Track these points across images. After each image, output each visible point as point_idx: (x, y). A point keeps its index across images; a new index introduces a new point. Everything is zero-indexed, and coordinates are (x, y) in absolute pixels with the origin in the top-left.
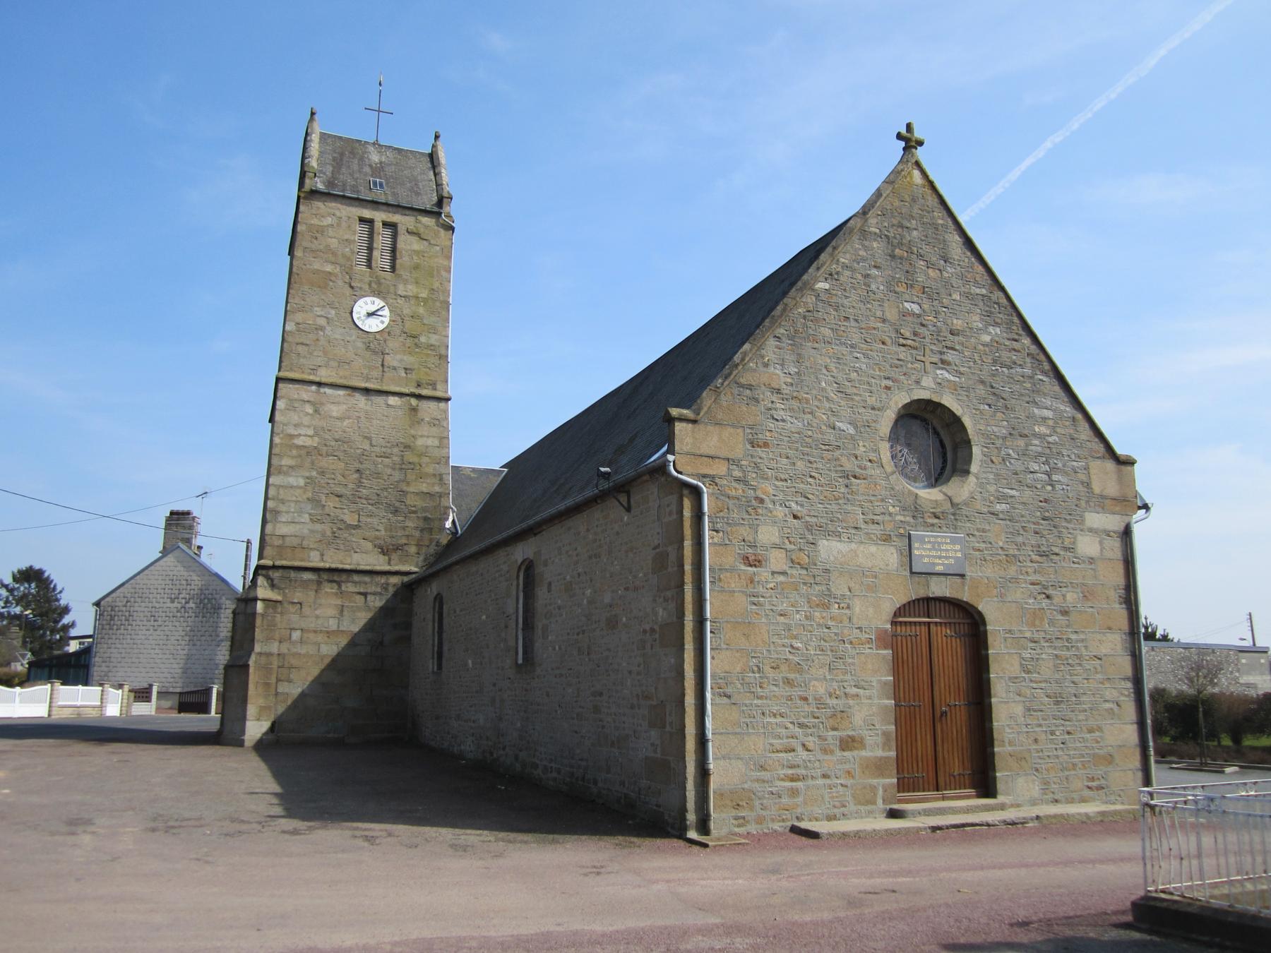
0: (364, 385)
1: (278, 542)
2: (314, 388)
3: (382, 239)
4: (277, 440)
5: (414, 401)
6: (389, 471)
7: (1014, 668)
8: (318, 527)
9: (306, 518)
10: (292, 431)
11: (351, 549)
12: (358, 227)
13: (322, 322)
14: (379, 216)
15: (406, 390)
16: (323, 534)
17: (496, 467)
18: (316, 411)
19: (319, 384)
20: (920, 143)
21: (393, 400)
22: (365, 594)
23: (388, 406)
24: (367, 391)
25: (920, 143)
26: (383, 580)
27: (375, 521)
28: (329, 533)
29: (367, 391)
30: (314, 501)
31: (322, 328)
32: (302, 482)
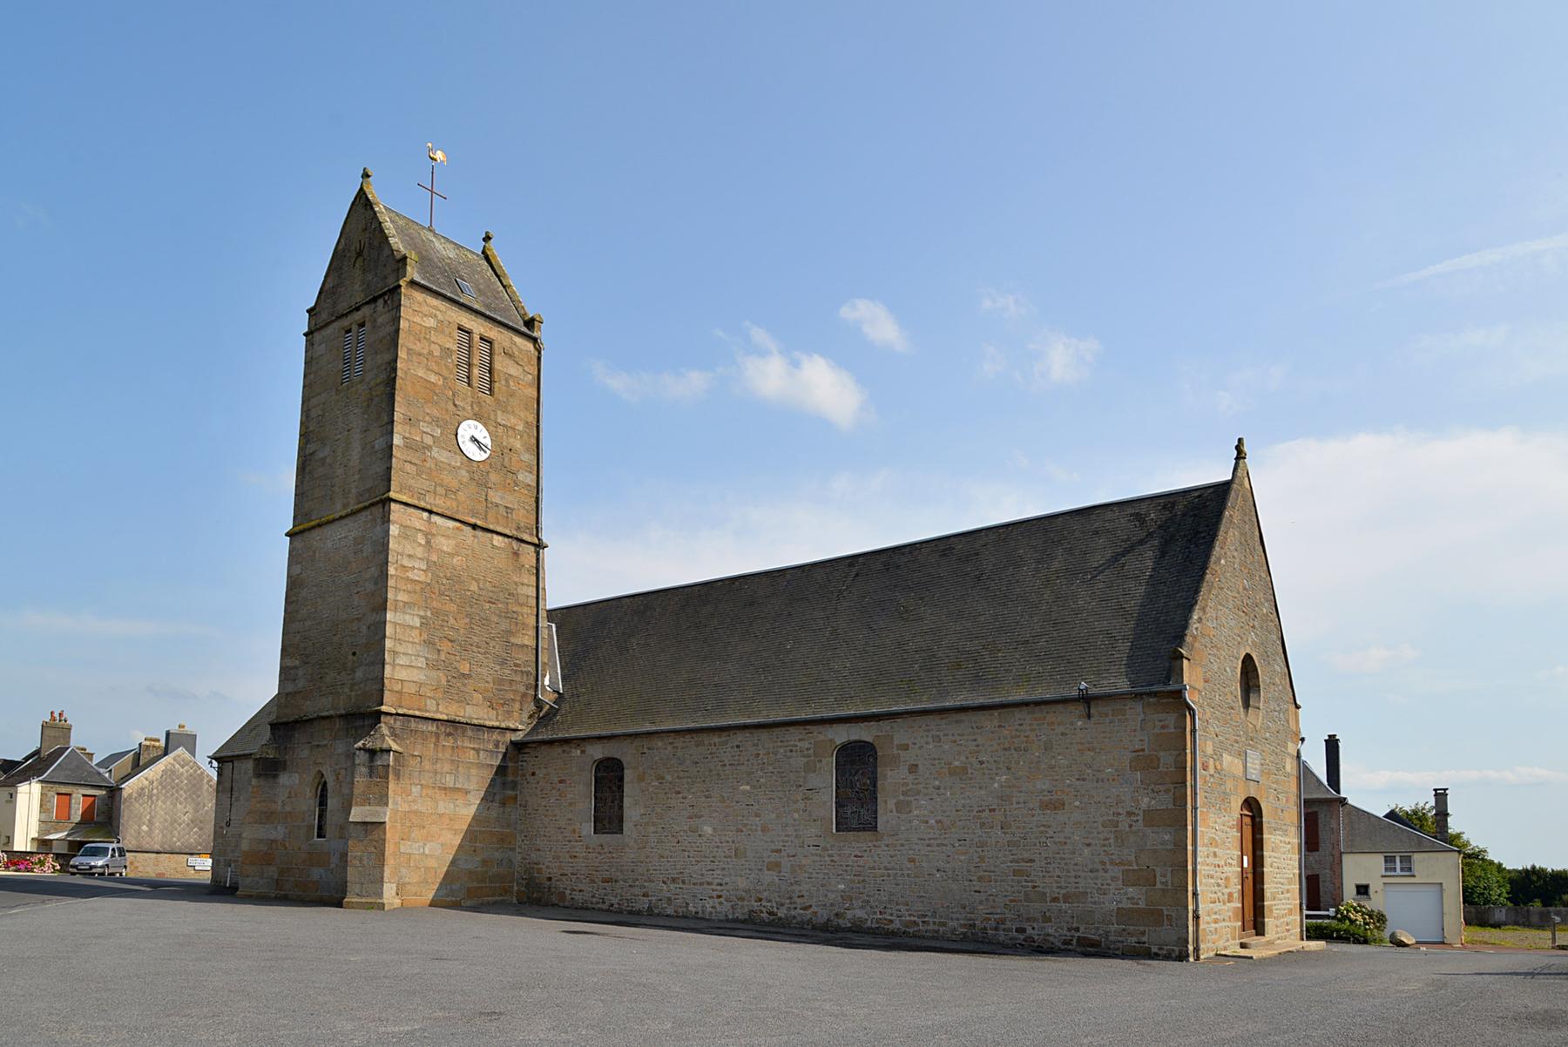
0: (472, 521)
1: (398, 687)
2: (425, 515)
3: (480, 353)
4: (528, 478)
5: (515, 544)
6: (495, 619)
7: (891, 805)
8: (434, 674)
9: (421, 663)
10: (406, 562)
11: (464, 701)
12: (456, 333)
13: (428, 440)
14: (478, 327)
15: (507, 532)
16: (439, 681)
17: (1508, 866)
18: (428, 542)
19: (431, 512)
20: (56, 729)
21: (497, 540)
22: (477, 751)
23: (494, 546)
24: (474, 527)
25: (56, 729)
26: (496, 736)
27: (484, 671)
28: (444, 682)
29: (474, 527)
30: (429, 643)
31: (429, 448)
32: (417, 622)
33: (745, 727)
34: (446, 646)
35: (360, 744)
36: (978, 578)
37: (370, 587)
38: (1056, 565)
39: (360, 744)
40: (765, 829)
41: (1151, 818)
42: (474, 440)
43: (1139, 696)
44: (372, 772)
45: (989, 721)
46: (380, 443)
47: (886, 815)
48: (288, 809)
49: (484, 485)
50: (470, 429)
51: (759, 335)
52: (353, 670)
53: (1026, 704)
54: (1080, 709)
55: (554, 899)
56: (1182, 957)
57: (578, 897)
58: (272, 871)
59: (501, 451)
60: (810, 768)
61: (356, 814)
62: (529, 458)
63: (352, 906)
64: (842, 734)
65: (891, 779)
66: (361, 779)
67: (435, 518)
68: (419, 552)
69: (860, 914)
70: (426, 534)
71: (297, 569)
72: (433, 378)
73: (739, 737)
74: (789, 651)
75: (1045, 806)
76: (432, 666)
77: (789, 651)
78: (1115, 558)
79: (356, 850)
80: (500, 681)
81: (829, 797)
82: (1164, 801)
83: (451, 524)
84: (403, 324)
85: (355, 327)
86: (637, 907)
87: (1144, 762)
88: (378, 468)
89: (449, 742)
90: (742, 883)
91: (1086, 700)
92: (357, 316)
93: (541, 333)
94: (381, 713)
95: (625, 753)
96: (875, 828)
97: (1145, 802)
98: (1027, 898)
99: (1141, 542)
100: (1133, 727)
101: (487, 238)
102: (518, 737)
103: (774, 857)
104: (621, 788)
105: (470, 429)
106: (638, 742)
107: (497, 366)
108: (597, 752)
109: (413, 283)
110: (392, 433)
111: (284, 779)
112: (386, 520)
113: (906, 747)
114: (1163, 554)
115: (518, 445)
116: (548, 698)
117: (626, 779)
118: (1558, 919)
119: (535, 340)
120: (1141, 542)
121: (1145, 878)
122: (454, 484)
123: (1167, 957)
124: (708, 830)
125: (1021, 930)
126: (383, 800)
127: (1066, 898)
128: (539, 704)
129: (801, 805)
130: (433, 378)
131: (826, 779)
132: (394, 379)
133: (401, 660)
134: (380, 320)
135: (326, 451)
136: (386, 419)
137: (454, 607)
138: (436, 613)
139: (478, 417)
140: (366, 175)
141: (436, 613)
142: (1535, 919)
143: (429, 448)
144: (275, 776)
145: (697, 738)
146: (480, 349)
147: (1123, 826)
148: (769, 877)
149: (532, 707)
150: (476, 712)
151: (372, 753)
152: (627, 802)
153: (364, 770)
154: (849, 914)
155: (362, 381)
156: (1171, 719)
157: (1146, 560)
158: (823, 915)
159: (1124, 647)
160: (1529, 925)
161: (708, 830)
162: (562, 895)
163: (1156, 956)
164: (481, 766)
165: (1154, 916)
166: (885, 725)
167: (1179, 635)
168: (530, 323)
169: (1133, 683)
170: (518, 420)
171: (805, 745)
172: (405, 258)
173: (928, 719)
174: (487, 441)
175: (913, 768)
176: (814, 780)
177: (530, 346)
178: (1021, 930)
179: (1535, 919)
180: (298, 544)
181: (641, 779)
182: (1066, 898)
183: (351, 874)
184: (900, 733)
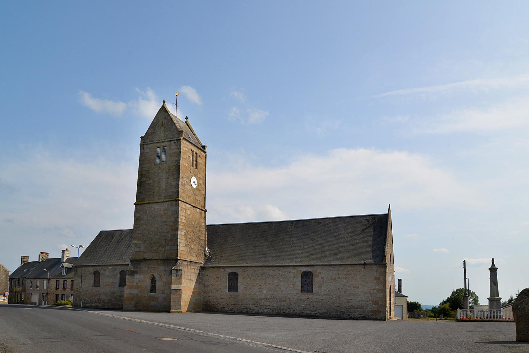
7: (317, 286)
24: (194, 207)
26: (198, 265)
27: (195, 247)
29: (194, 207)
30: (186, 240)
33: (277, 266)
34: (189, 240)
35: (173, 268)
36: (330, 231)
37: (171, 224)
38: (349, 230)
39: (173, 268)
40: (282, 292)
41: (378, 291)
42: (194, 182)
43: (376, 264)
44: (177, 275)
45: (342, 268)
46: (174, 183)
47: (315, 288)
48: (139, 285)
49: (195, 195)
50: (194, 179)
51: (149, 88)
52: (165, 247)
53: (351, 265)
54: (363, 266)
55: (215, 310)
56: (385, 320)
57: (223, 309)
58: (133, 303)
59: (199, 185)
60: (294, 277)
61: (173, 287)
62: (203, 186)
63: (173, 312)
64: (304, 269)
65: (317, 281)
66: (174, 277)
67: (187, 205)
68: (184, 214)
69: (309, 312)
70: (185, 209)
71: (139, 215)
72: (187, 165)
73: (274, 268)
74: (282, 246)
75: (354, 287)
76: (187, 246)
77: (282, 246)
78: (364, 230)
79: (173, 297)
80: (198, 250)
81: (300, 284)
82: (381, 287)
83: (190, 206)
84: (182, 150)
85: (162, 147)
86: (243, 311)
87: (377, 278)
88: (175, 190)
89: (189, 267)
90: (275, 305)
91: (365, 264)
92: (163, 144)
93: (207, 150)
94: (178, 259)
95: (239, 271)
96: (312, 292)
97: (377, 287)
98: (350, 308)
99: (369, 227)
100: (374, 271)
101: (187, 118)
102: (202, 265)
103: (285, 299)
104: (237, 280)
105: (194, 179)
106: (243, 268)
107: (198, 161)
108: (230, 270)
109: (184, 138)
110: (179, 181)
111: (137, 276)
112: (177, 205)
113: (320, 273)
114: (375, 231)
115: (201, 183)
116: (207, 254)
117: (239, 278)
118: (422, 316)
119: (205, 152)
120: (369, 227)
121: (377, 303)
122: (190, 195)
123: (382, 320)
124: (265, 292)
125: (349, 315)
126: (180, 283)
127: (359, 308)
128: (205, 255)
129: (292, 286)
130: (187, 165)
131: (299, 280)
132: (179, 166)
133: (181, 245)
134: (172, 147)
135: (151, 181)
136: (176, 177)
137: (190, 229)
138: (187, 231)
139: (195, 176)
140: (164, 102)
141: (187, 231)
142: (416, 316)
143: (186, 185)
144: (134, 275)
145: (262, 268)
146: (195, 155)
147: (372, 292)
148: (284, 303)
149: (204, 257)
150: (194, 259)
151: (177, 270)
152: (239, 284)
153: (175, 275)
154: (306, 312)
155: (165, 164)
156: (383, 270)
157: (371, 231)
158: (298, 312)
159: (370, 252)
160: (415, 318)
161: (265, 292)
162: (218, 309)
163: (379, 320)
164: (195, 273)
165: (379, 311)
166: (315, 267)
167: (383, 251)
168: (204, 147)
169: (375, 261)
170: (201, 176)
171: (293, 271)
172: (182, 131)
173: (326, 267)
174: (196, 182)
175: (322, 278)
176: (296, 280)
177: (203, 154)
178: (349, 315)
179: (416, 316)
180: (139, 207)
181: (244, 278)
182: (359, 308)
183: (172, 304)
184: (319, 269)
